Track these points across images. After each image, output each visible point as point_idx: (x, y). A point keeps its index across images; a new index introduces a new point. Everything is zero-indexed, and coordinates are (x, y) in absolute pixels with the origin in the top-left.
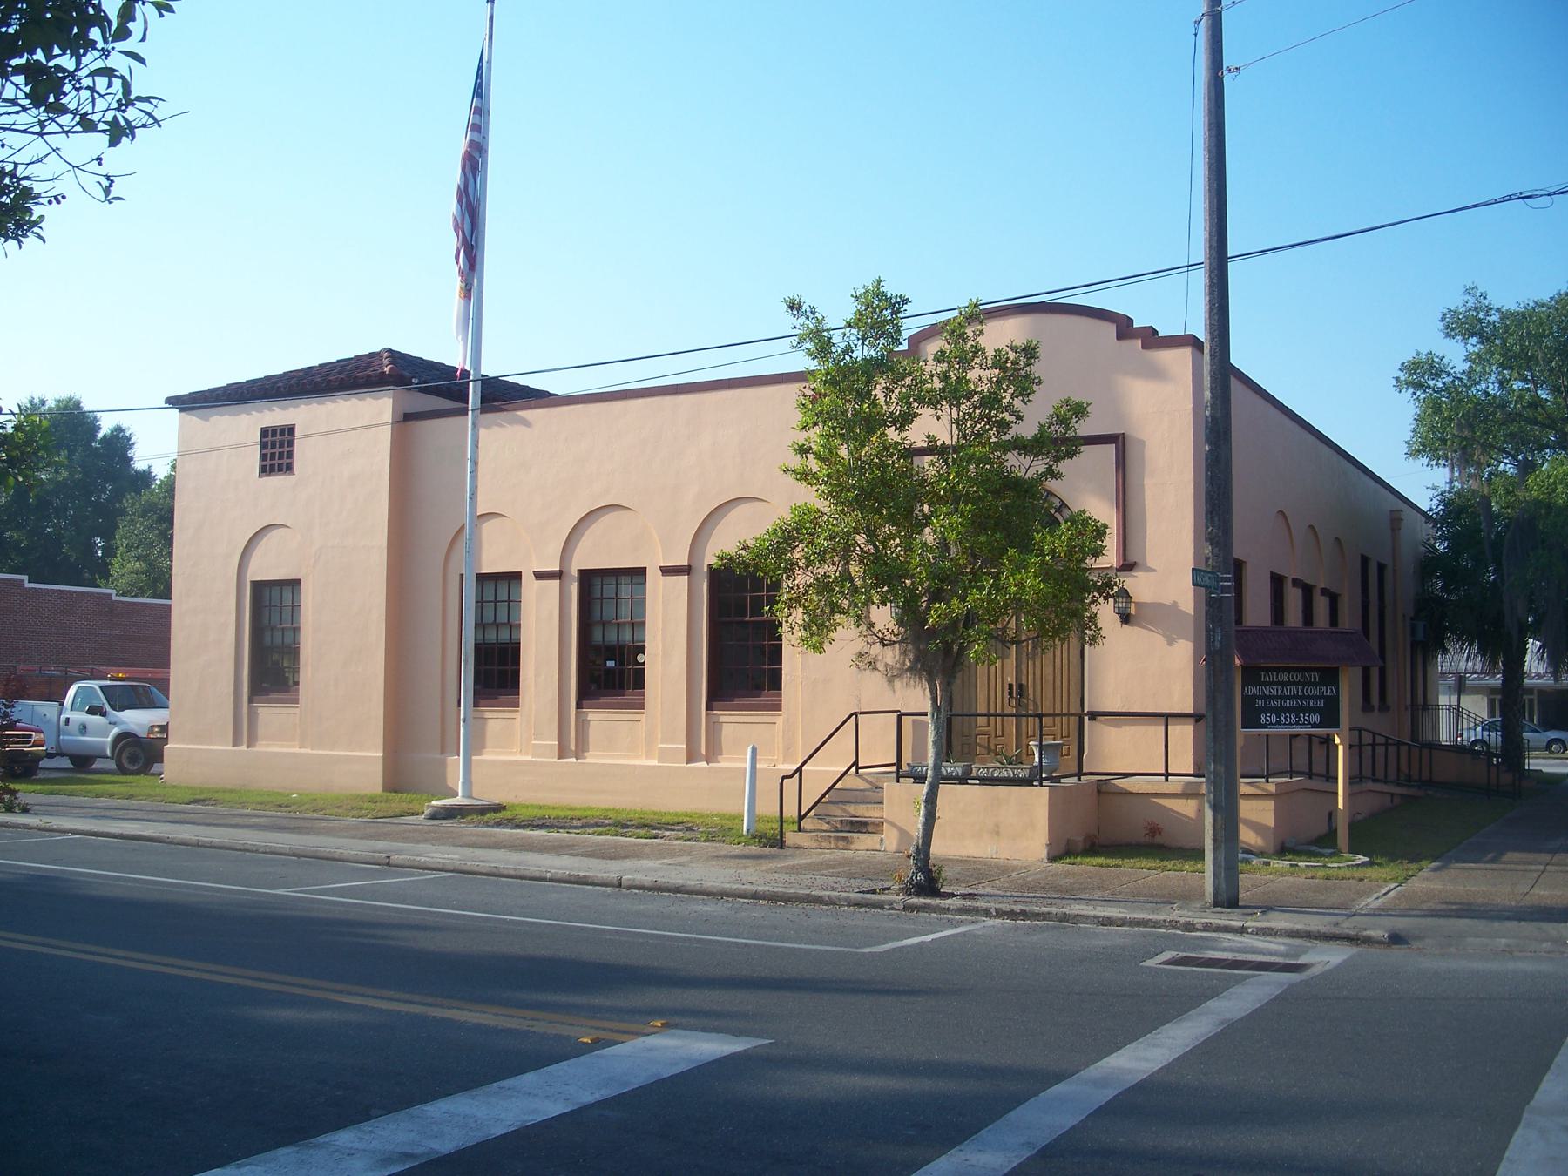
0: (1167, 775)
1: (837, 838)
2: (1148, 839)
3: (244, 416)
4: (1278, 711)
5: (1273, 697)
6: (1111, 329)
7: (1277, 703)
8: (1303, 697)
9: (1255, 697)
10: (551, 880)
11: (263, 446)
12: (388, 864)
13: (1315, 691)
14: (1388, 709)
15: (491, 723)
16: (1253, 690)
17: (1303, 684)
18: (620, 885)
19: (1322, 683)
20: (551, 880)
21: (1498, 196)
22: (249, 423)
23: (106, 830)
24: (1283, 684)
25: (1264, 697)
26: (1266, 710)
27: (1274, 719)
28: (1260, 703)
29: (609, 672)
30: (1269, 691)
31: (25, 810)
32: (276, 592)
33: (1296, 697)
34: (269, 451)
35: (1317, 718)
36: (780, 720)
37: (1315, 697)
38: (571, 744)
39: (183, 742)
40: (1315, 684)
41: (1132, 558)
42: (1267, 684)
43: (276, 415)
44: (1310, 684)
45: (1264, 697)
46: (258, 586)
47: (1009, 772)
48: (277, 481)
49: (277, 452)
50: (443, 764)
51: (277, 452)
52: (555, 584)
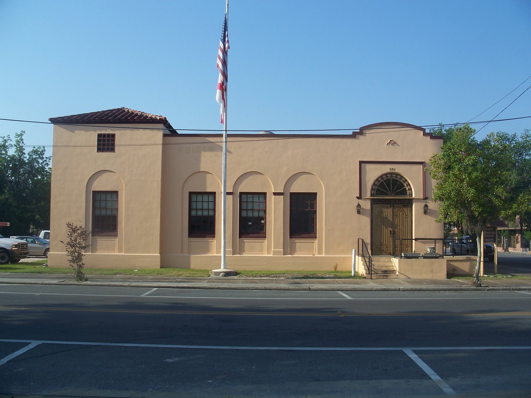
1: (383, 276)
2: (453, 272)
3: (83, 132)
10: (375, 291)
11: (113, 145)
12: (310, 290)
15: (297, 244)
18: (400, 290)
20: (375, 291)
23: (154, 285)
29: (251, 225)
31: (87, 280)
32: (103, 197)
34: (110, 147)
36: (316, 241)
38: (288, 249)
39: (58, 251)
46: (95, 193)
49: (106, 144)
50: (189, 258)
52: (282, 197)
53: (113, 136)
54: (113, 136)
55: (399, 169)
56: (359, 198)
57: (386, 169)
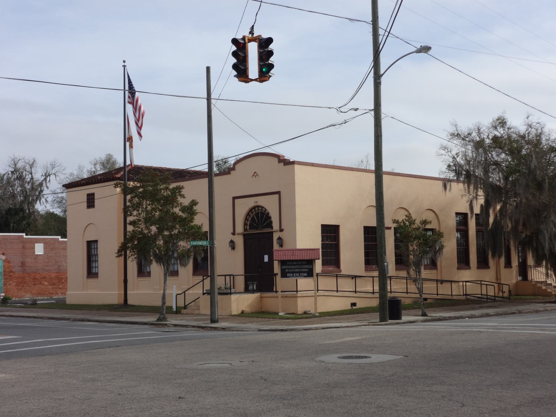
0: (437, 294)
4: (293, 273)
5: (291, 269)
6: (276, 160)
7: (293, 270)
8: (301, 269)
9: (285, 269)
13: (305, 266)
14: (96, 275)
16: (284, 267)
17: (301, 265)
19: (307, 264)
21: (326, 126)
22: (82, 193)
24: (294, 265)
25: (288, 269)
26: (289, 272)
27: (292, 275)
28: (287, 270)
30: (290, 267)
33: (299, 268)
35: (306, 274)
37: (305, 268)
40: (305, 265)
41: (282, 228)
42: (289, 265)
43: (90, 189)
44: (303, 265)
45: (288, 269)
47: (543, 301)
48: (91, 210)
49: (91, 201)
51: (91, 201)
53: (489, 268)
54: (489, 268)
55: (262, 201)
56: (234, 234)
57: (251, 203)
